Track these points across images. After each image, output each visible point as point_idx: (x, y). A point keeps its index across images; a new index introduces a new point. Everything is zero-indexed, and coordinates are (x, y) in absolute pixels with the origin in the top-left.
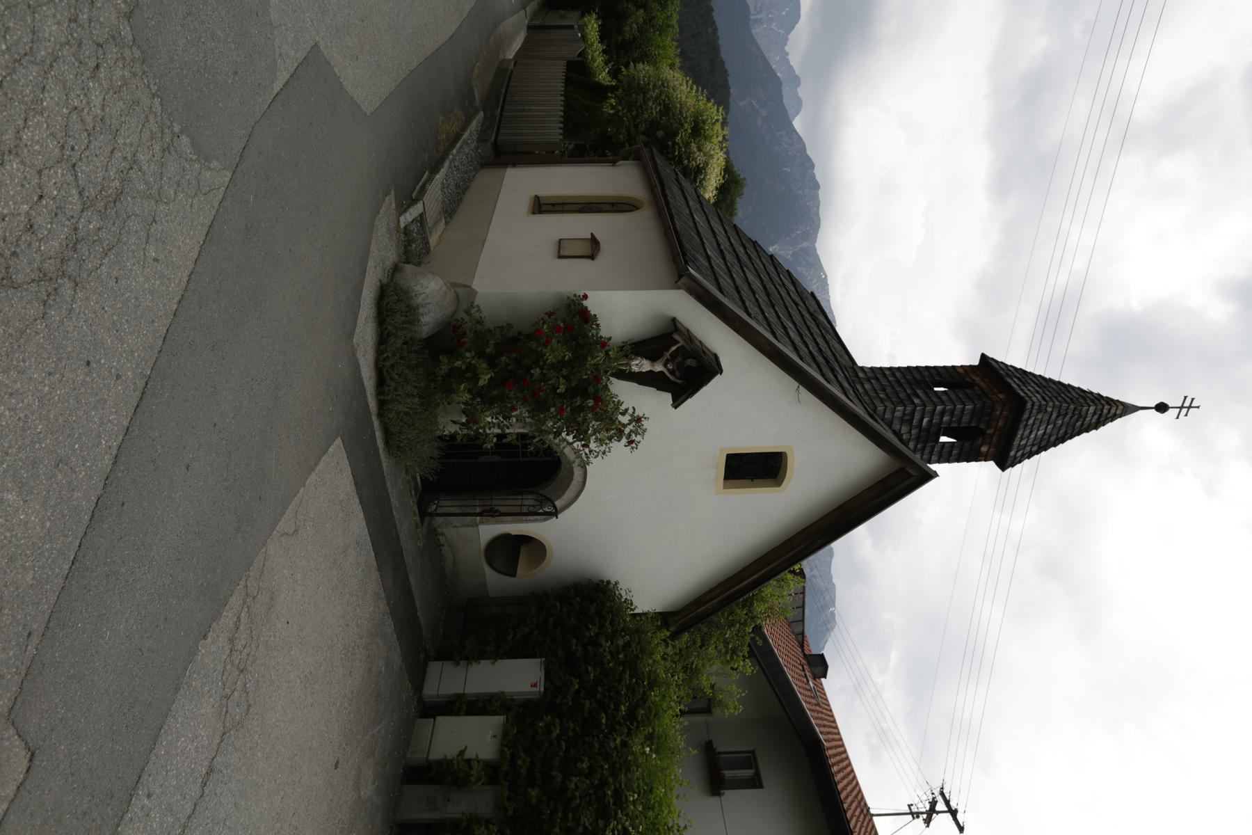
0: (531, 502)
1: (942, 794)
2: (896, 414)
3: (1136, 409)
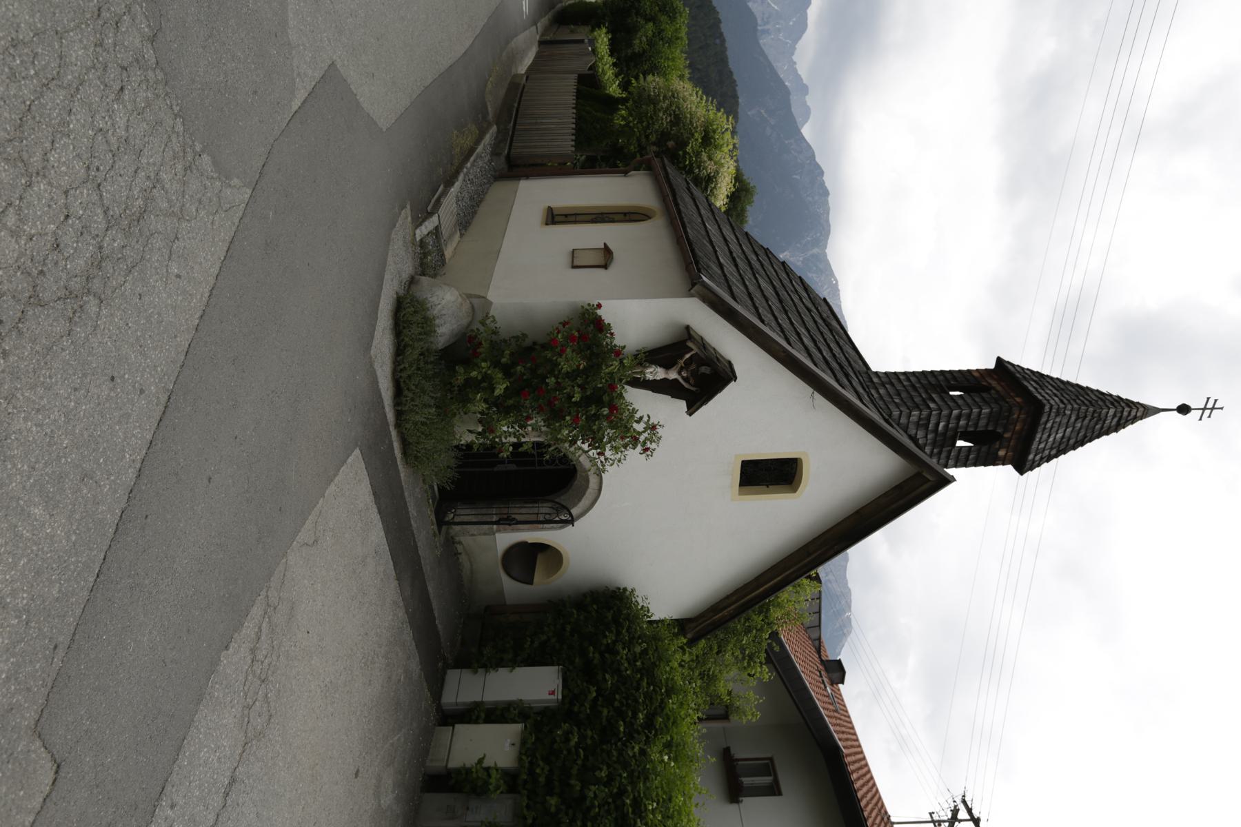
1: (964, 802)
2: (911, 418)
3: (1157, 411)
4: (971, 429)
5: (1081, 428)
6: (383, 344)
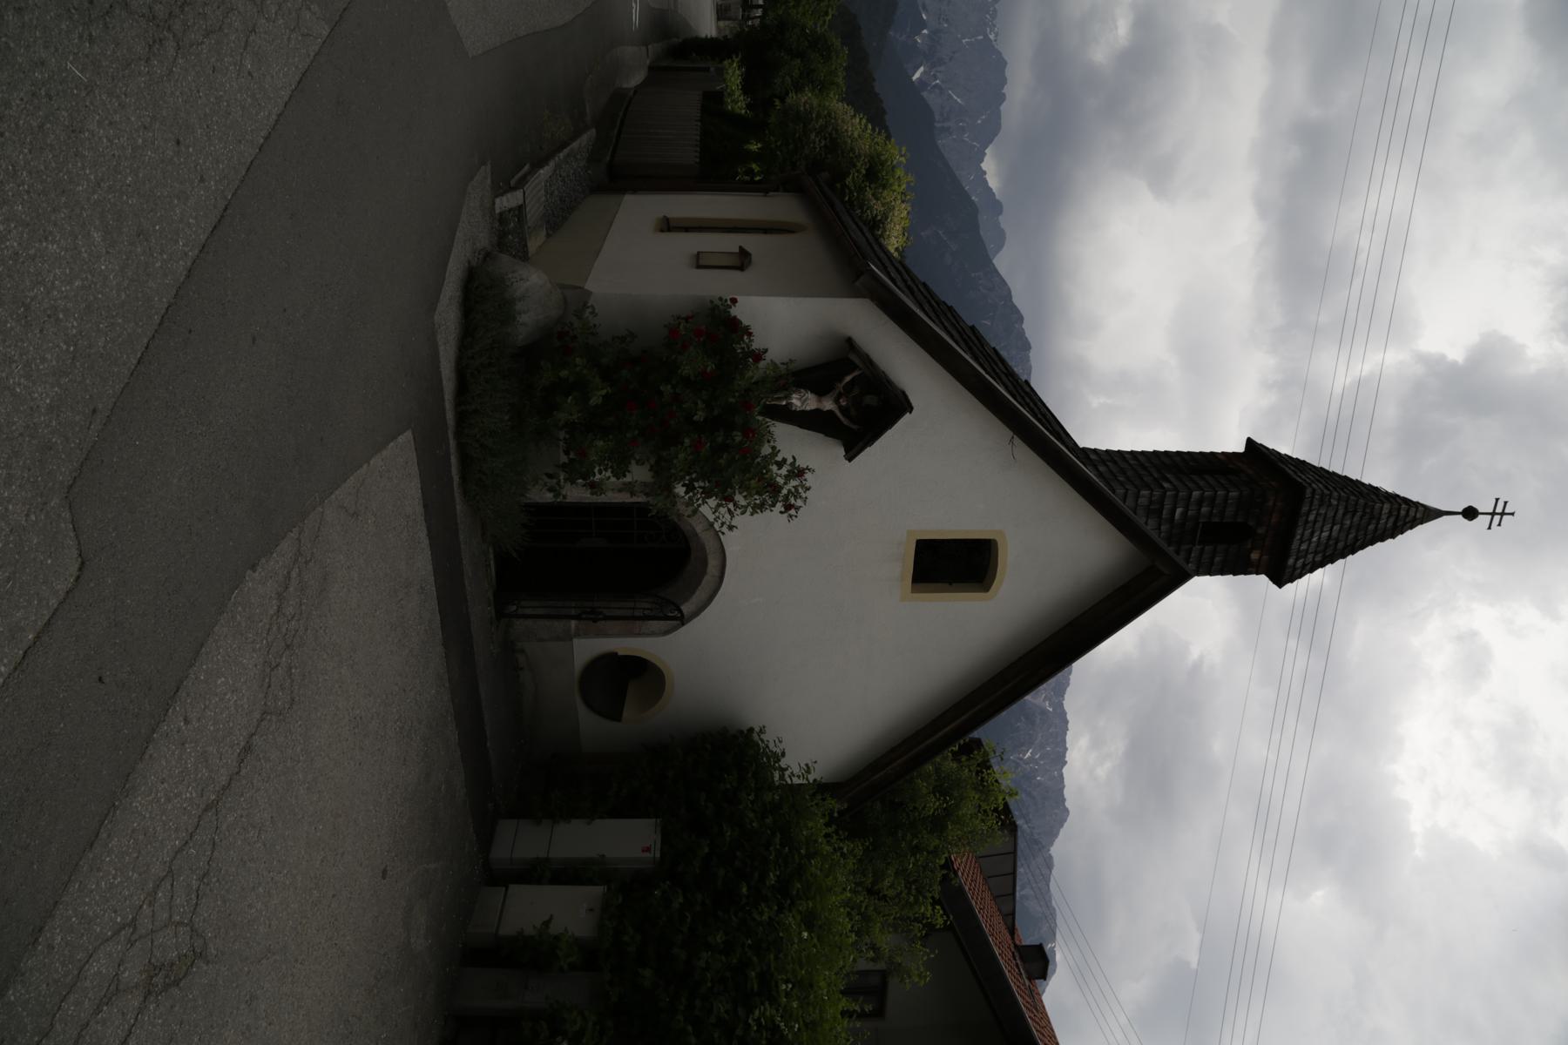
0: (647, 606)
2: (1140, 500)
3: (1430, 514)
4: (1216, 520)
5: (1350, 528)
6: (448, 316)
